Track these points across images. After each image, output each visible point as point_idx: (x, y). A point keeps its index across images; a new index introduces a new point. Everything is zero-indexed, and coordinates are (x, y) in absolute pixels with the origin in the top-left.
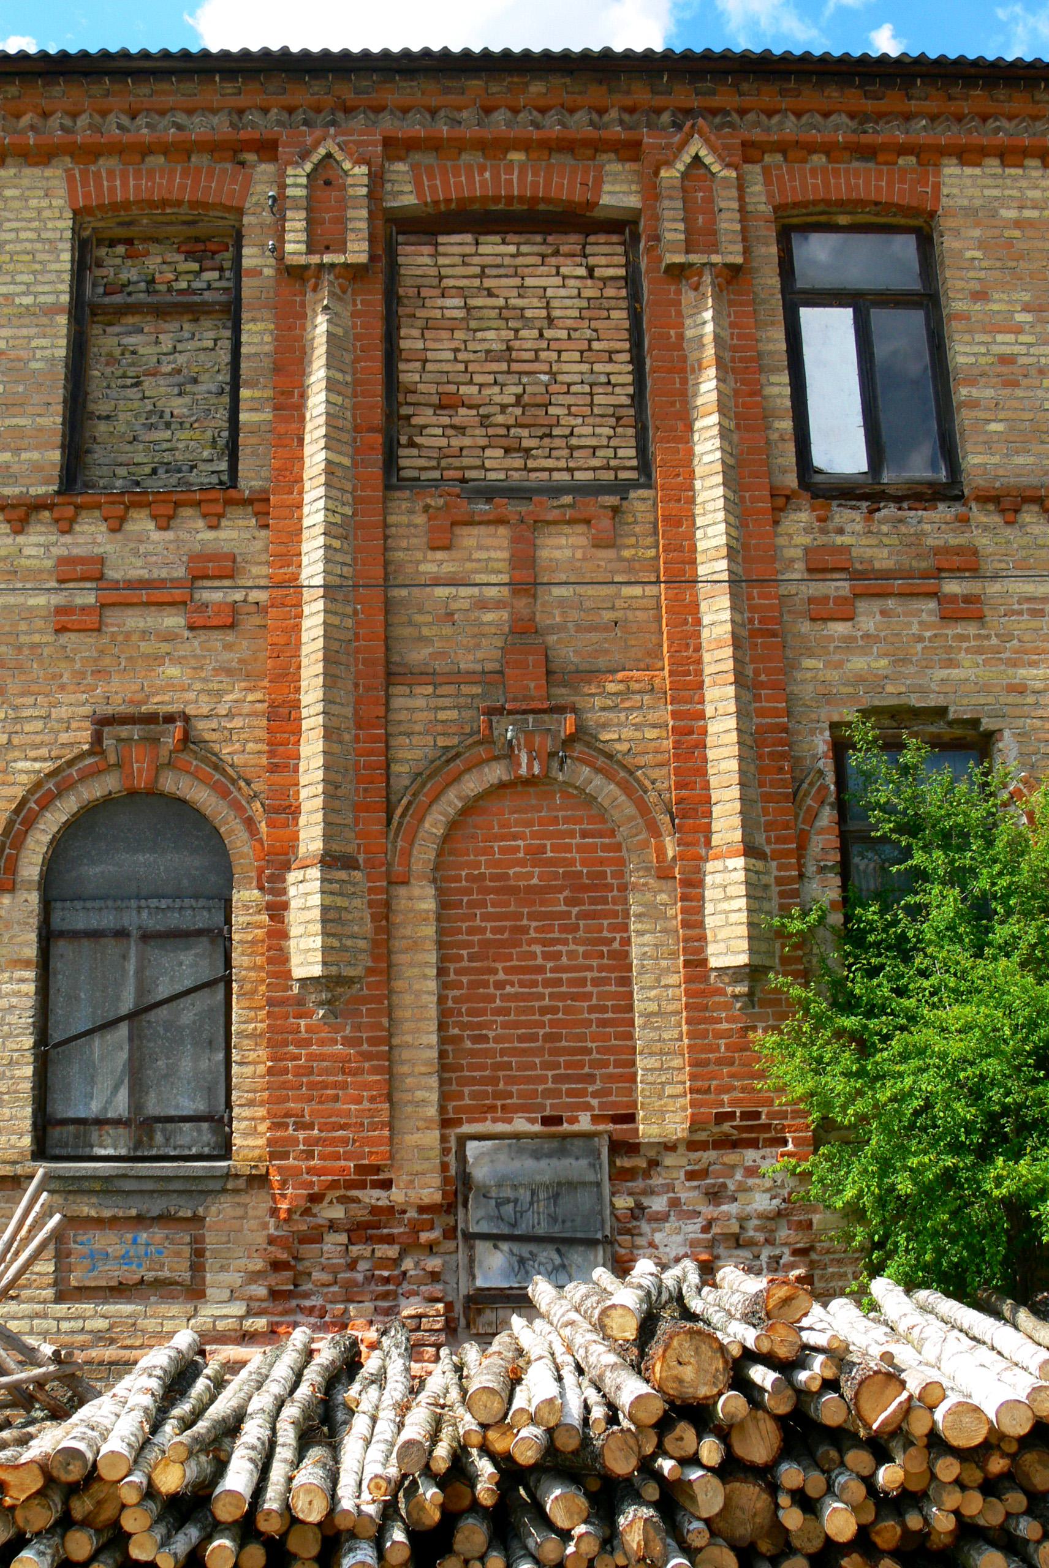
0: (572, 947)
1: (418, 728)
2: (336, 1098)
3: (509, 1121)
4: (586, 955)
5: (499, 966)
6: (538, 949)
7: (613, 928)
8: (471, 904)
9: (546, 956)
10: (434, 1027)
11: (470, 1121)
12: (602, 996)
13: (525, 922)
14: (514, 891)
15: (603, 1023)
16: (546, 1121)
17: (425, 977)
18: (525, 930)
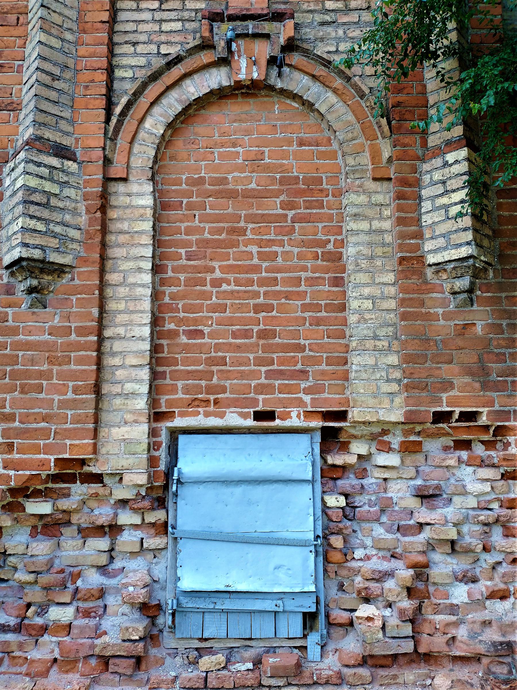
0: (287, 248)
1: (143, 38)
2: (40, 389)
3: (222, 415)
4: (300, 256)
5: (216, 264)
6: (254, 249)
7: (328, 231)
8: (190, 207)
9: (262, 256)
10: (147, 318)
11: (183, 415)
12: (315, 295)
13: (242, 224)
14: (232, 195)
15: (318, 322)
16: (259, 416)
17: (140, 270)
18: (243, 232)
